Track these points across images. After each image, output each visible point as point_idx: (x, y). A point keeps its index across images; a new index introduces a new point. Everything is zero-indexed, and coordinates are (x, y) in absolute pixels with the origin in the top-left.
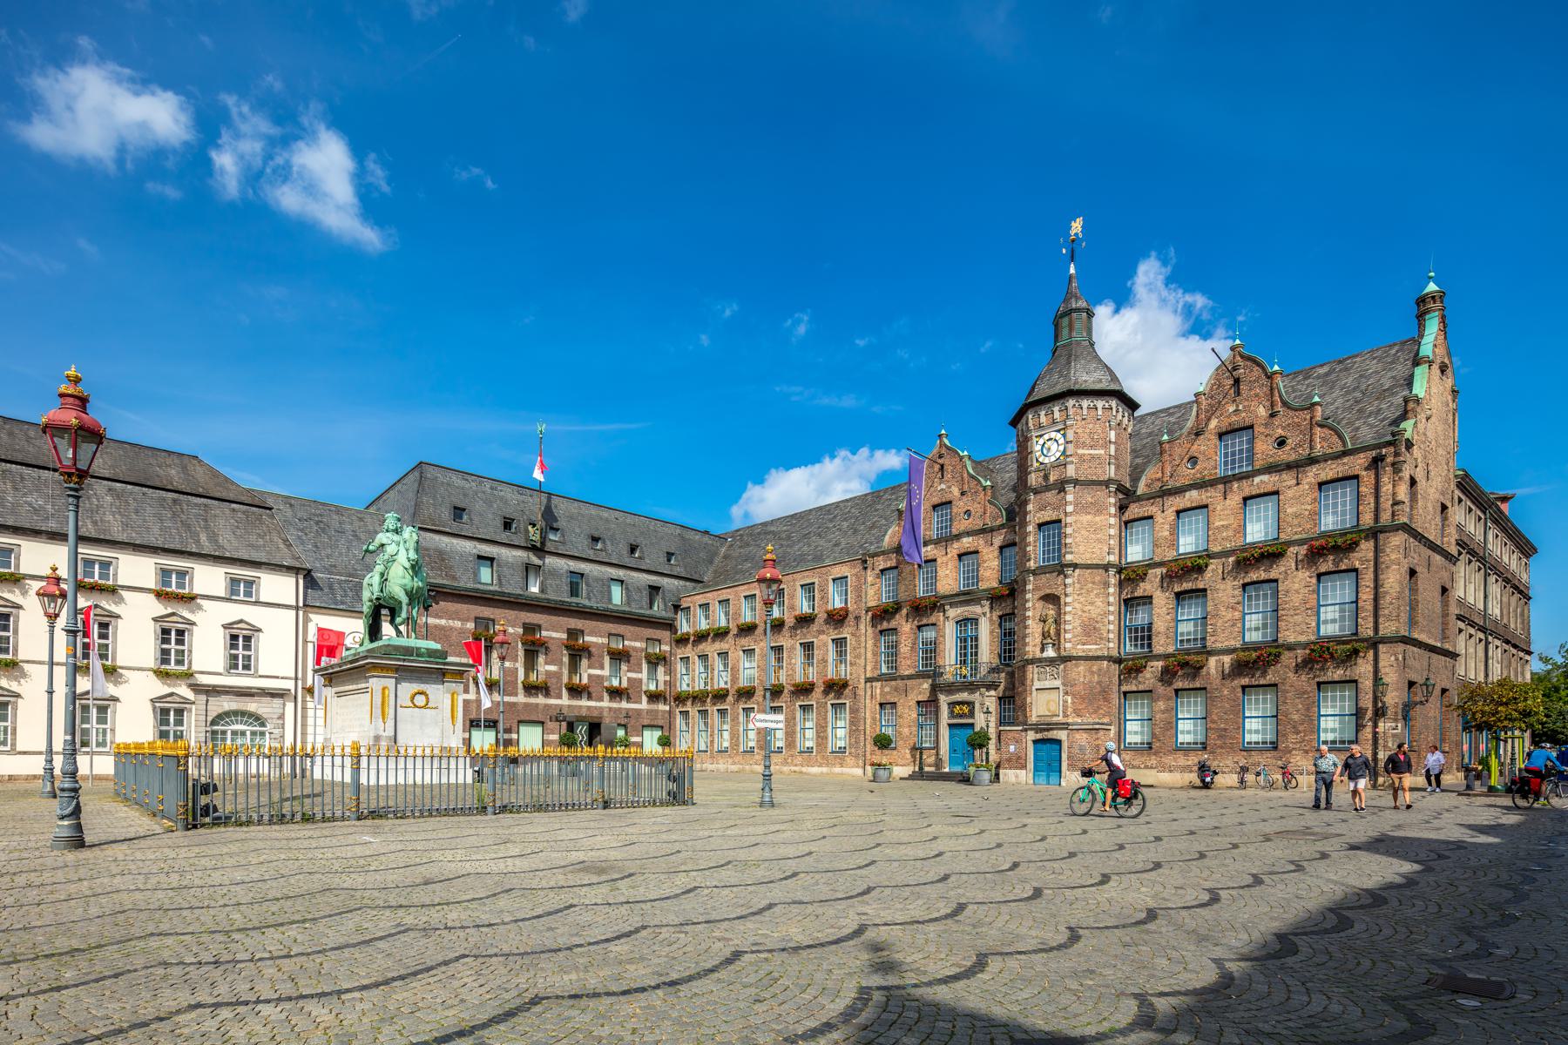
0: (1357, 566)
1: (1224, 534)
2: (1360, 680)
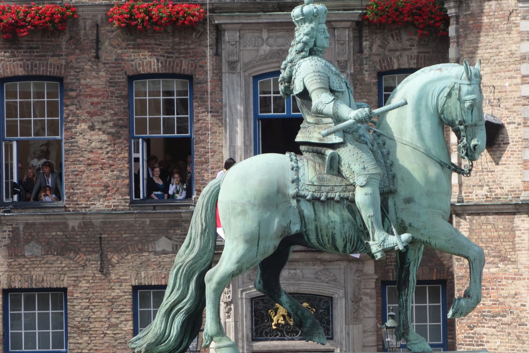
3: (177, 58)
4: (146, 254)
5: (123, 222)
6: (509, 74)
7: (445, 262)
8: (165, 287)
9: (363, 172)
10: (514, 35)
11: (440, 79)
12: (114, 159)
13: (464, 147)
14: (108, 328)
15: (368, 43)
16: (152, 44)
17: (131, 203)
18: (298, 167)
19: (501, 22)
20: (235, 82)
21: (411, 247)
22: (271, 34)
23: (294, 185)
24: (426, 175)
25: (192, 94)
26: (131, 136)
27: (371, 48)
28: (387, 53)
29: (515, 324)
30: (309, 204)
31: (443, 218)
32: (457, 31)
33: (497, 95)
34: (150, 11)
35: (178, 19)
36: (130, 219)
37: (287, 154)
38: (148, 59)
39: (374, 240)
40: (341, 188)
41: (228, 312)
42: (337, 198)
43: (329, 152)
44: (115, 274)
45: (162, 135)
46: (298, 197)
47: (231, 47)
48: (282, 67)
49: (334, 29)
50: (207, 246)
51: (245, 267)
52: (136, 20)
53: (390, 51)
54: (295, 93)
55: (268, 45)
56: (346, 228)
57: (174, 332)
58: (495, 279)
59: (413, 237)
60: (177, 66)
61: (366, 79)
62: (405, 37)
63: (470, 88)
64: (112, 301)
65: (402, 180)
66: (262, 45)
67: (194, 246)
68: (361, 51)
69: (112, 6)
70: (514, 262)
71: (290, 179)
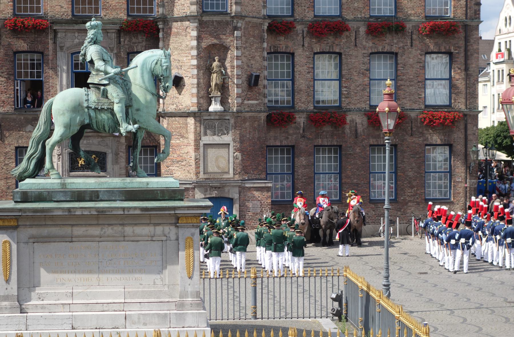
0: (452, 51)
1: (356, 5)
2: (454, 145)
3: (36, 44)
4: (22, 132)
5: (11, 118)
6: (186, 55)
7: (156, 138)
8: (27, 147)
9: (117, 97)
10: (188, 37)
11: (152, 56)
12: (7, 89)
13: (163, 86)
14: (4, 166)
15: (123, 39)
16: (24, 37)
17: (15, 109)
18: (88, 94)
19: (183, 31)
20: (63, 56)
21: (139, 131)
22: (79, 34)
23: (86, 102)
24: (146, 99)
25: (43, 61)
26: (15, 79)
27: (124, 42)
28: (131, 44)
29: (187, 165)
30: (93, 111)
31: (153, 118)
32: (163, 35)
33: (180, 64)
34: (24, 23)
35: (37, 27)
36: (14, 117)
37: (84, 88)
38: (23, 44)
39: (122, 127)
40: (107, 104)
41: (59, 159)
42: (106, 108)
43: (102, 88)
44: (8, 141)
45: (29, 79)
46: (88, 107)
47: (61, 40)
48: (82, 49)
49: (108, 33)
50: (47, 129)
51: (64, 138)
52: (17, 26)
53: (133, 43)
54: (87, 61)
55: (78, 39)
56: (110, 122)
57: (32, 167)
58: (178, 145)
59: (139, 126)
60: (36, 47)
61: (122, 56)
62: (140, 37)
63: (166, 60)
64: (6, 153)
65: (135, 100)
66: (75, 39)
67: (41, 129)
68: (120, 43)
69: (6, 20)
70: (187, 138)
71: (85, 99)
